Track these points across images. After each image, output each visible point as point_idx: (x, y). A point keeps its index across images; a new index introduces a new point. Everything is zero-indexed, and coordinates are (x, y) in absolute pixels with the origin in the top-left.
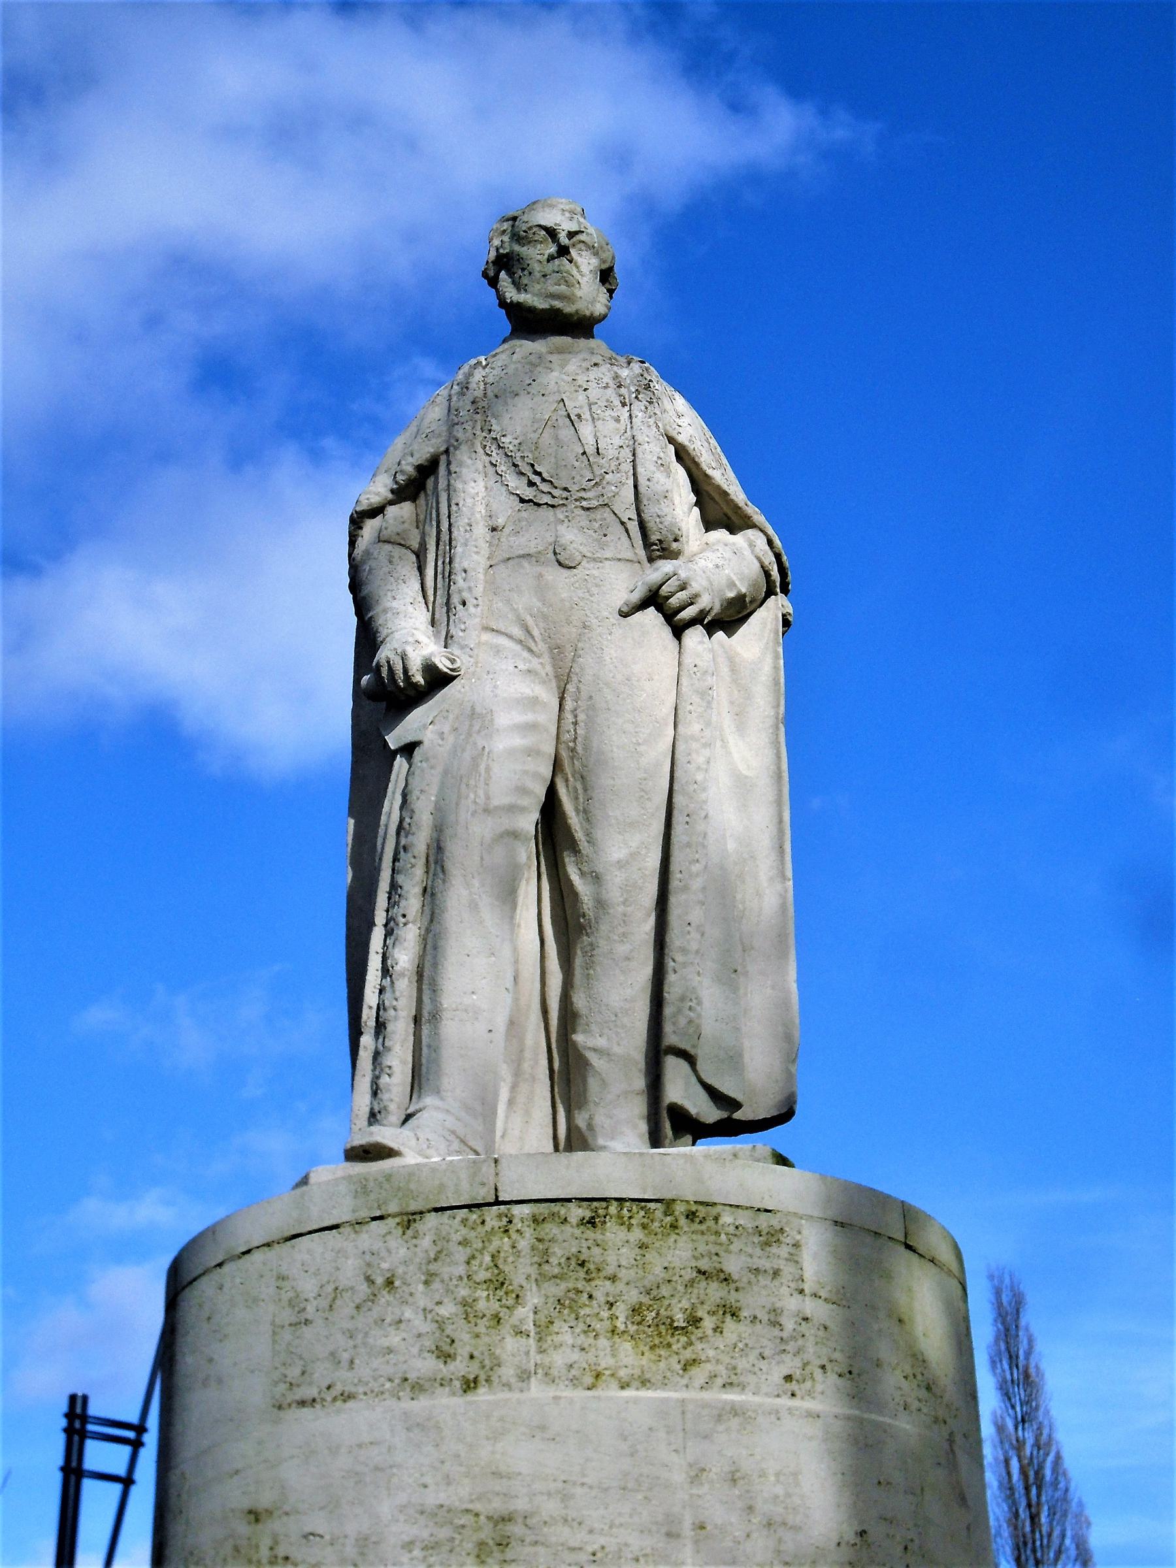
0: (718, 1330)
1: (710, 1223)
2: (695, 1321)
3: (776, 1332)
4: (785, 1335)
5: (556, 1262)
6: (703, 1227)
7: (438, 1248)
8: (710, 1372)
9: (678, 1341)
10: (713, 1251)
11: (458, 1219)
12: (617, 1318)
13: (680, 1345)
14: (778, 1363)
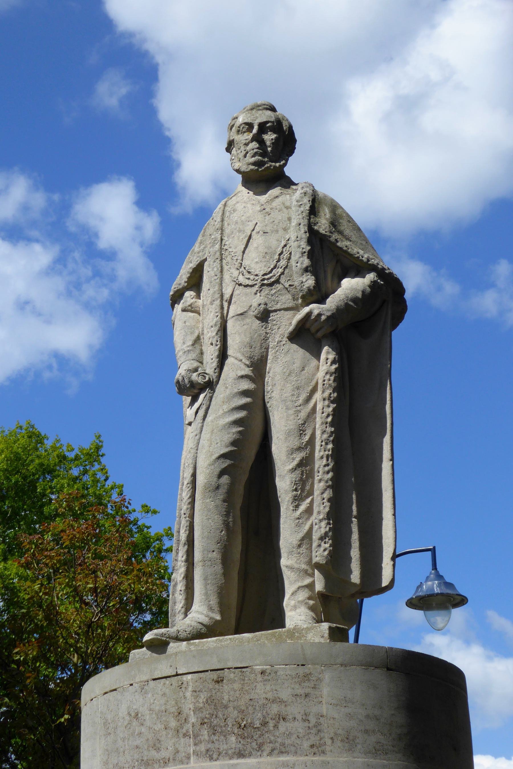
0: (276, 726)
1: (273, 675)
2: (265, 724)
3: (306, 724)
4: (311, 725)
5: (201, 701)
6: (270, 678)
7: (154, 698)
8: (272, 748)
9: (257, 734)
10: (274, 689)
11: (162, 684)
12: (228, 726)
13: (257, 736)
14: (307, 739)
